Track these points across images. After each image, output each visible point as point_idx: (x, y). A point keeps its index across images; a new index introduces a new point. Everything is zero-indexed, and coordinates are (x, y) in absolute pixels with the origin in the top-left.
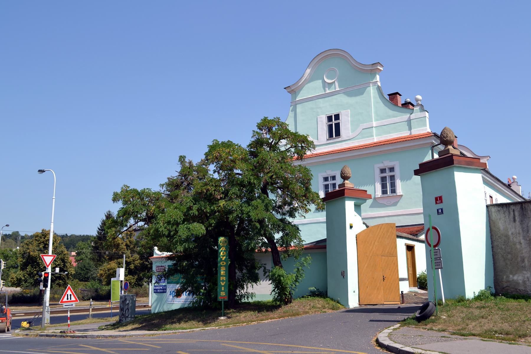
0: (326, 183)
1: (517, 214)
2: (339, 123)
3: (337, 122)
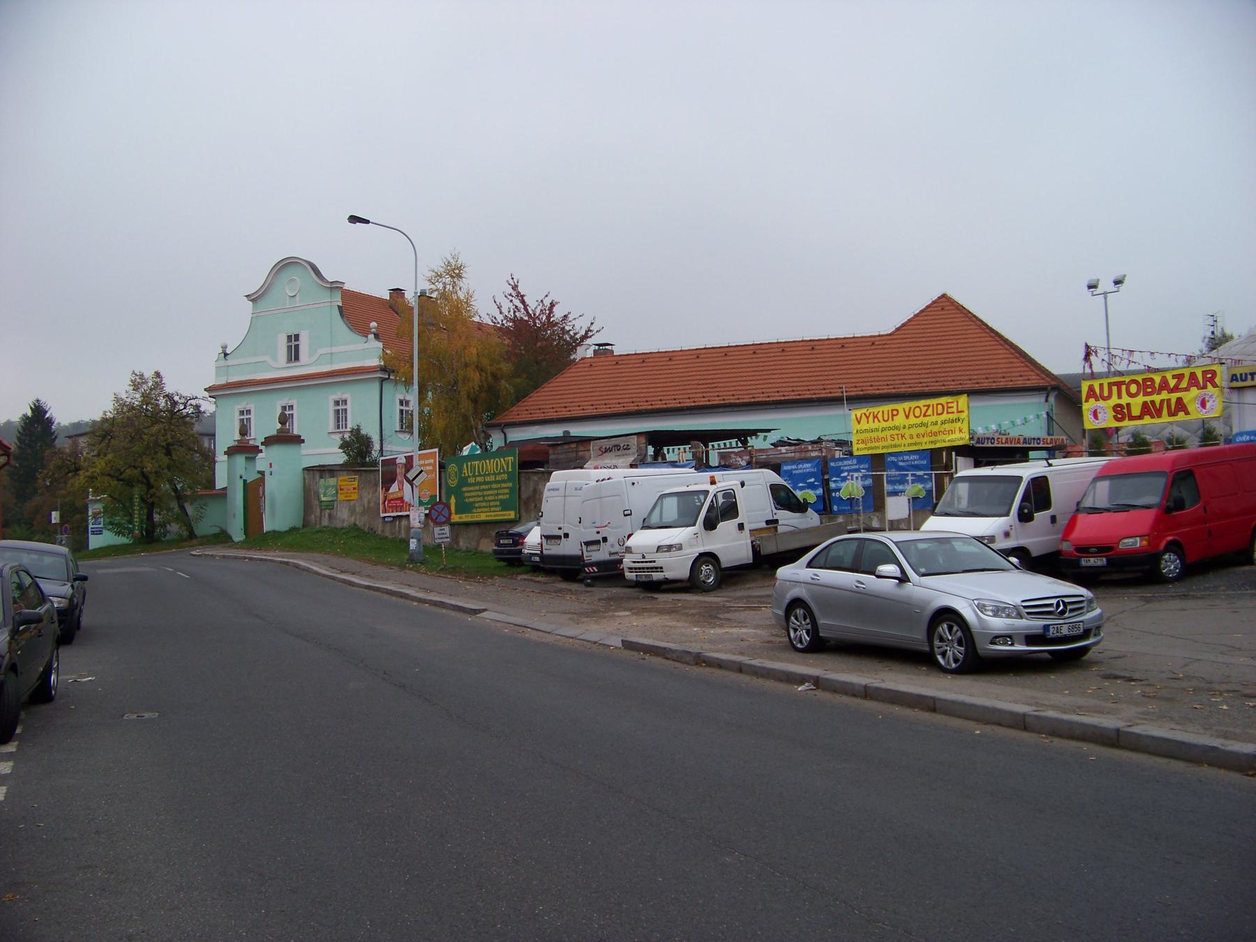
0: (242, 417)
2: (298, 345)
3: (297, 343)
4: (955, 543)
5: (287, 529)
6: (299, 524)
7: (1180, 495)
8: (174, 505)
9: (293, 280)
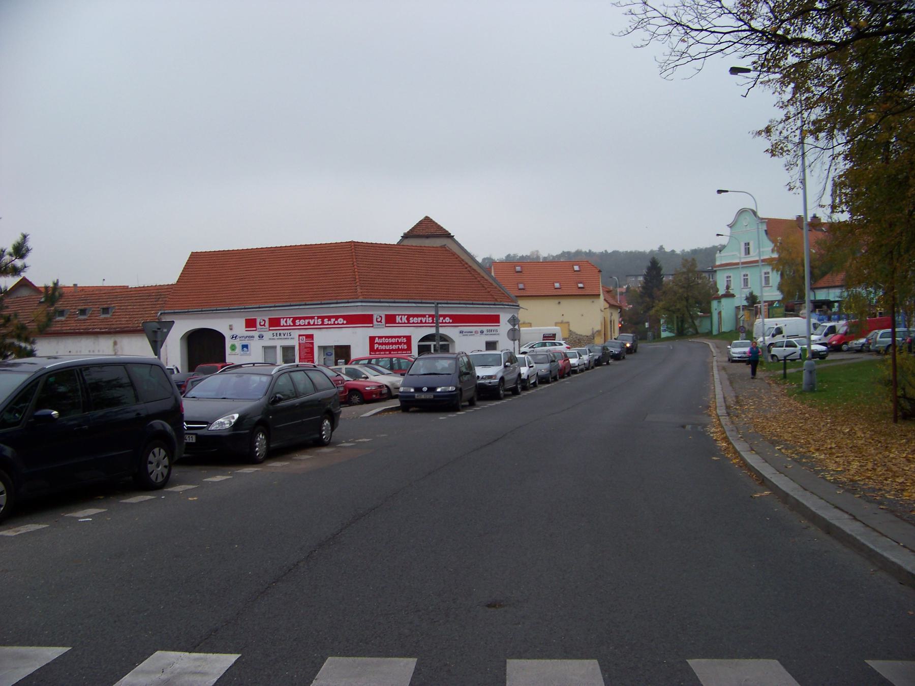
4: (344, 373)
5: (729, 331)
6: (734, 329)
7: (774, 329)
8: (690, 320)
9: (746, 218)
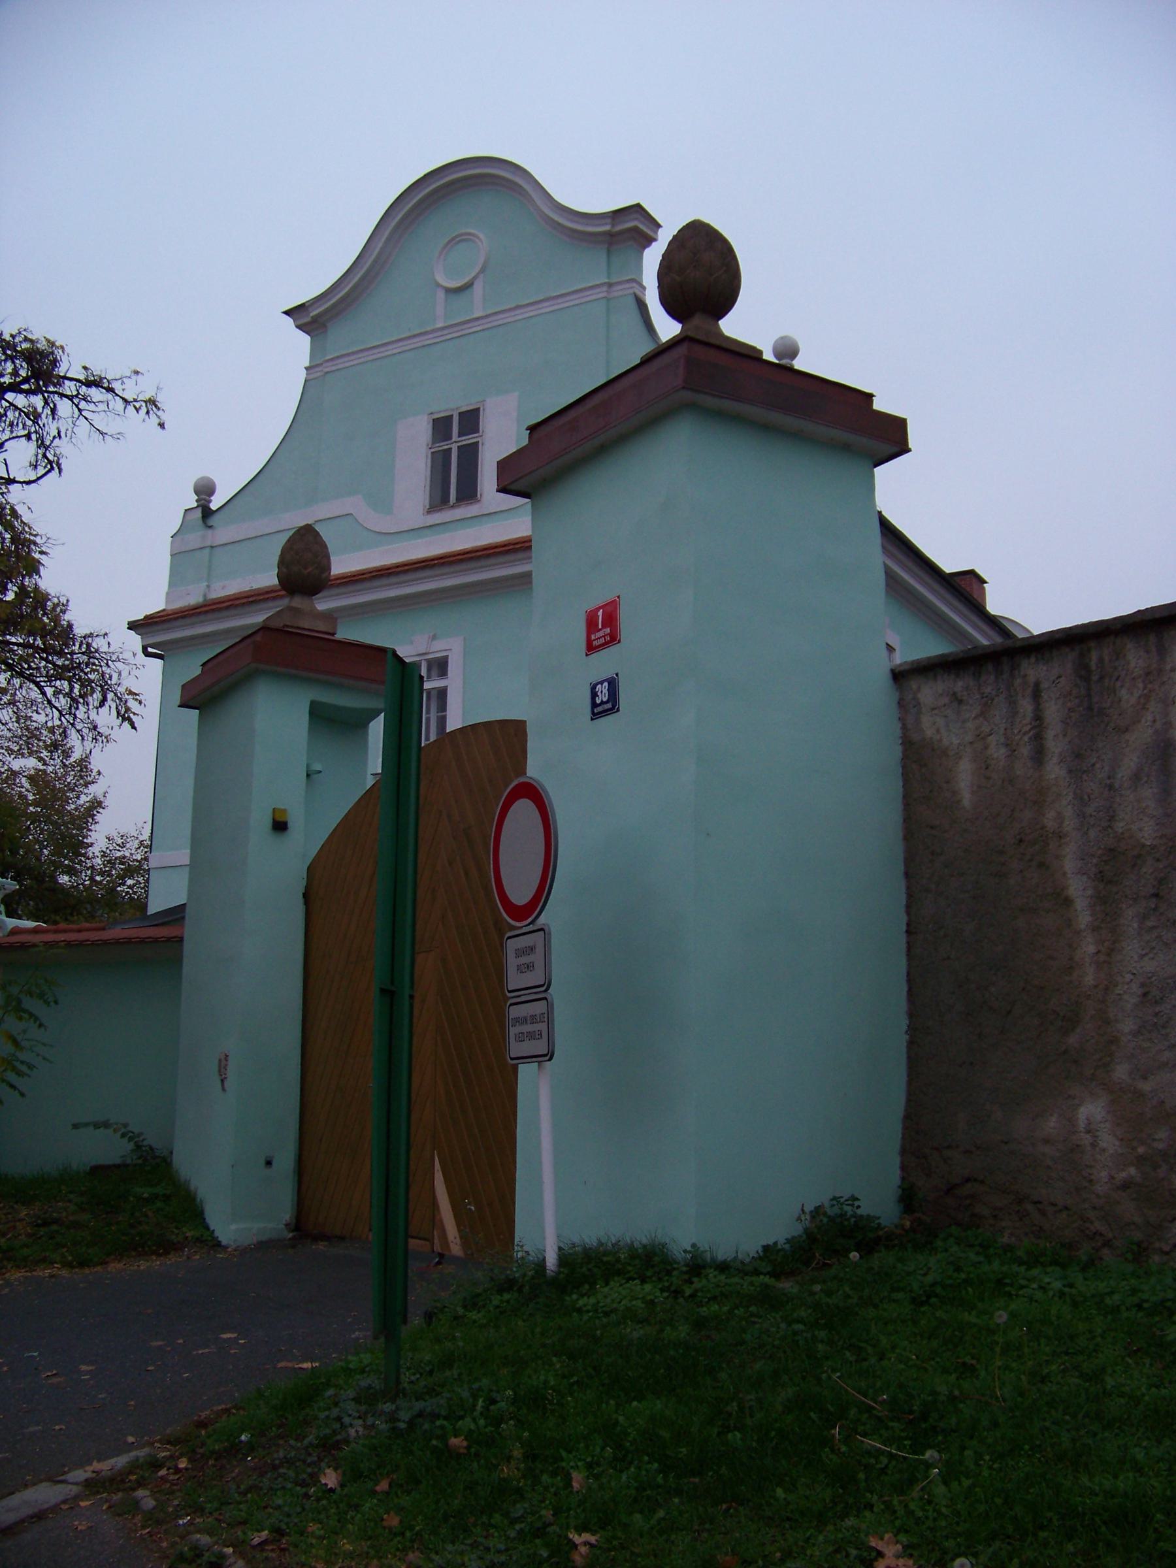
1: (1053, 711)
3: (468, 440)
